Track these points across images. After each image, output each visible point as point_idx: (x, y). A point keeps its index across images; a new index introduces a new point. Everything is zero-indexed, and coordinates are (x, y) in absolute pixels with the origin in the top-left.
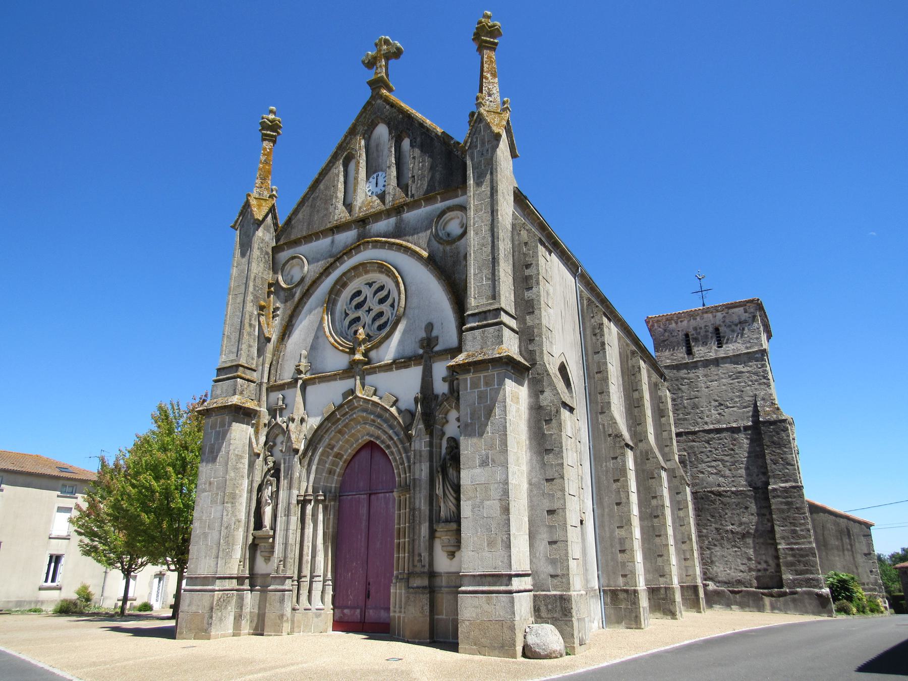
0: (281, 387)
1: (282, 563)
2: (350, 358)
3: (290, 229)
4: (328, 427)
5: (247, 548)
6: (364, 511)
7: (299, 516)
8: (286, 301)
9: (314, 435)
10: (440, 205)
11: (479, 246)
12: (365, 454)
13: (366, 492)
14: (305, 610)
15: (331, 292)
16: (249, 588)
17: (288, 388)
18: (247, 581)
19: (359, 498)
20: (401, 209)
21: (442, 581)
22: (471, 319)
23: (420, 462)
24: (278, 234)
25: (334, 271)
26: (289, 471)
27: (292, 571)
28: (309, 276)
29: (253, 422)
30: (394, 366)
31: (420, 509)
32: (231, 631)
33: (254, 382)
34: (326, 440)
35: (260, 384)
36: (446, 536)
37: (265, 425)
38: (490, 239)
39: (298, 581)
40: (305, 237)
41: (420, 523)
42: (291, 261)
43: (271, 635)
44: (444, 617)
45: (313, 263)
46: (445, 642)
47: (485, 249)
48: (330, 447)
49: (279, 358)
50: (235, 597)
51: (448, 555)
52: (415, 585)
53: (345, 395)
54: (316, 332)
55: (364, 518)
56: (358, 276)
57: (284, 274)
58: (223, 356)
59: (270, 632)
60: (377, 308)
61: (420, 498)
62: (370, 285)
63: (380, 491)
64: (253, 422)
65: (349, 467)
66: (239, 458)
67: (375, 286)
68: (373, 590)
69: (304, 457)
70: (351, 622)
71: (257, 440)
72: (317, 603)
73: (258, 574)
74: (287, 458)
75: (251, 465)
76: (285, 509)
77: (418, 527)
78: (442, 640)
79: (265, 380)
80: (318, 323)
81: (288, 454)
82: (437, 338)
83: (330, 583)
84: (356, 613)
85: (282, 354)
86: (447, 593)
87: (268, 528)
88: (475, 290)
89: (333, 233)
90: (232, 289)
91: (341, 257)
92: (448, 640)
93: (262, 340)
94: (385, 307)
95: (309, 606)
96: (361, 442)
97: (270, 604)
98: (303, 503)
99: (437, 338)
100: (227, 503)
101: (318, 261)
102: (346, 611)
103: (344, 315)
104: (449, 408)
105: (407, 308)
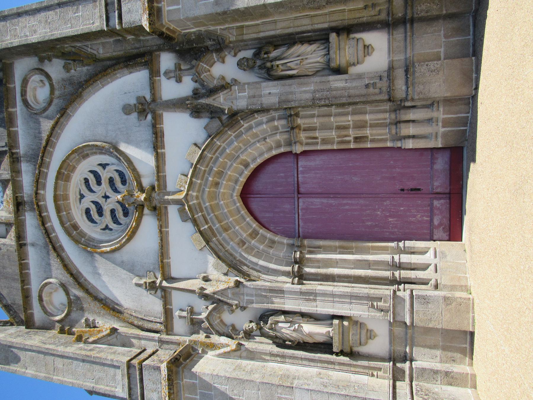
0: (168, 313)
1: (375, 304)
2: (147, 215)
3: (15, 307)
4: (217, 243)
5: (355, 363)
6: (317, 202)
7: (317, 283)
8: (82, 309)
9: (223, 261)
10: (19, 109)
11: (47, 26)
12: (255, 205)
13: (296, 199)
14: (436, 272)
15: (77, 242)
16: (408, 363)
17: (171, 305)
18: (399, 365)
19: (302, 209)
20: (15, 156)
21: (399, 60)
22: (111, 23)
23: (260, 96)
24: (17, 323)
25: (59, 241)
26: (262, 296)
27: (386, 291)
28: (60, 276)
29: (200, 352)
30: (159, 151)
31: (314, 92)
32: (469, 391)
33: (157, 350)
34: (232, 246)
35: (161, 342)
36: (345, 49)
37: (207, 337)
38: (43, 14)
39: (399, 283)
40: (23, 281)
41: (330, 90)
42: (45, 303)
43: (473, 317)
44: (442, 50)
45: (50, 271)
46: (474, 45)
47: (51, 18)
48: (241, 245)
49: (137, 317)
50: (421, 383)
51: (368, 54)
52: (404, 88)
53: (184, 218)
54: (116, 265)
55: (325, 201)
56: (68, 209)
57: (55, 314)
58: (117, 390)
59: (468, 319)
60: (105, 187)
61: (301, 93)
62: (82, 196)
63: (296, 179)
64: (200, 352)
65: (267, 225)
66: (239, 367)
67: (85, 191)
68: (411, 184)
69: (249, 276)
70: (450, 215)
71: (223, 346)
72: (428, 258)
73: (390, 350)
74: (246, 298)
75: (252, 356)
76: (308, 300)
77: (334, 92)
78: (471, 49)
79: (157, 335)
80: (108, 262)
81: (242, 297)
82: (138, 98)
83: (401, 244)
84: (438, 205)
85: (134, 314)
86: (413, 49)
87: (330, 329)
88: (86, 25)
89: (25, 245)
90: (47, 375)
91: (46, 229)
92: (471, 41)
93: (112, 339)
94: (105, 175)
95: (432, 268)
96: (239, 204)
97: (430, 320)
98: (301, 277)
99: (138, 98)
100: (292, 383)
101: (49, 264)
102: (436, 222)
103: (107, 231)
104: (208, 73)
105: (105, 140)
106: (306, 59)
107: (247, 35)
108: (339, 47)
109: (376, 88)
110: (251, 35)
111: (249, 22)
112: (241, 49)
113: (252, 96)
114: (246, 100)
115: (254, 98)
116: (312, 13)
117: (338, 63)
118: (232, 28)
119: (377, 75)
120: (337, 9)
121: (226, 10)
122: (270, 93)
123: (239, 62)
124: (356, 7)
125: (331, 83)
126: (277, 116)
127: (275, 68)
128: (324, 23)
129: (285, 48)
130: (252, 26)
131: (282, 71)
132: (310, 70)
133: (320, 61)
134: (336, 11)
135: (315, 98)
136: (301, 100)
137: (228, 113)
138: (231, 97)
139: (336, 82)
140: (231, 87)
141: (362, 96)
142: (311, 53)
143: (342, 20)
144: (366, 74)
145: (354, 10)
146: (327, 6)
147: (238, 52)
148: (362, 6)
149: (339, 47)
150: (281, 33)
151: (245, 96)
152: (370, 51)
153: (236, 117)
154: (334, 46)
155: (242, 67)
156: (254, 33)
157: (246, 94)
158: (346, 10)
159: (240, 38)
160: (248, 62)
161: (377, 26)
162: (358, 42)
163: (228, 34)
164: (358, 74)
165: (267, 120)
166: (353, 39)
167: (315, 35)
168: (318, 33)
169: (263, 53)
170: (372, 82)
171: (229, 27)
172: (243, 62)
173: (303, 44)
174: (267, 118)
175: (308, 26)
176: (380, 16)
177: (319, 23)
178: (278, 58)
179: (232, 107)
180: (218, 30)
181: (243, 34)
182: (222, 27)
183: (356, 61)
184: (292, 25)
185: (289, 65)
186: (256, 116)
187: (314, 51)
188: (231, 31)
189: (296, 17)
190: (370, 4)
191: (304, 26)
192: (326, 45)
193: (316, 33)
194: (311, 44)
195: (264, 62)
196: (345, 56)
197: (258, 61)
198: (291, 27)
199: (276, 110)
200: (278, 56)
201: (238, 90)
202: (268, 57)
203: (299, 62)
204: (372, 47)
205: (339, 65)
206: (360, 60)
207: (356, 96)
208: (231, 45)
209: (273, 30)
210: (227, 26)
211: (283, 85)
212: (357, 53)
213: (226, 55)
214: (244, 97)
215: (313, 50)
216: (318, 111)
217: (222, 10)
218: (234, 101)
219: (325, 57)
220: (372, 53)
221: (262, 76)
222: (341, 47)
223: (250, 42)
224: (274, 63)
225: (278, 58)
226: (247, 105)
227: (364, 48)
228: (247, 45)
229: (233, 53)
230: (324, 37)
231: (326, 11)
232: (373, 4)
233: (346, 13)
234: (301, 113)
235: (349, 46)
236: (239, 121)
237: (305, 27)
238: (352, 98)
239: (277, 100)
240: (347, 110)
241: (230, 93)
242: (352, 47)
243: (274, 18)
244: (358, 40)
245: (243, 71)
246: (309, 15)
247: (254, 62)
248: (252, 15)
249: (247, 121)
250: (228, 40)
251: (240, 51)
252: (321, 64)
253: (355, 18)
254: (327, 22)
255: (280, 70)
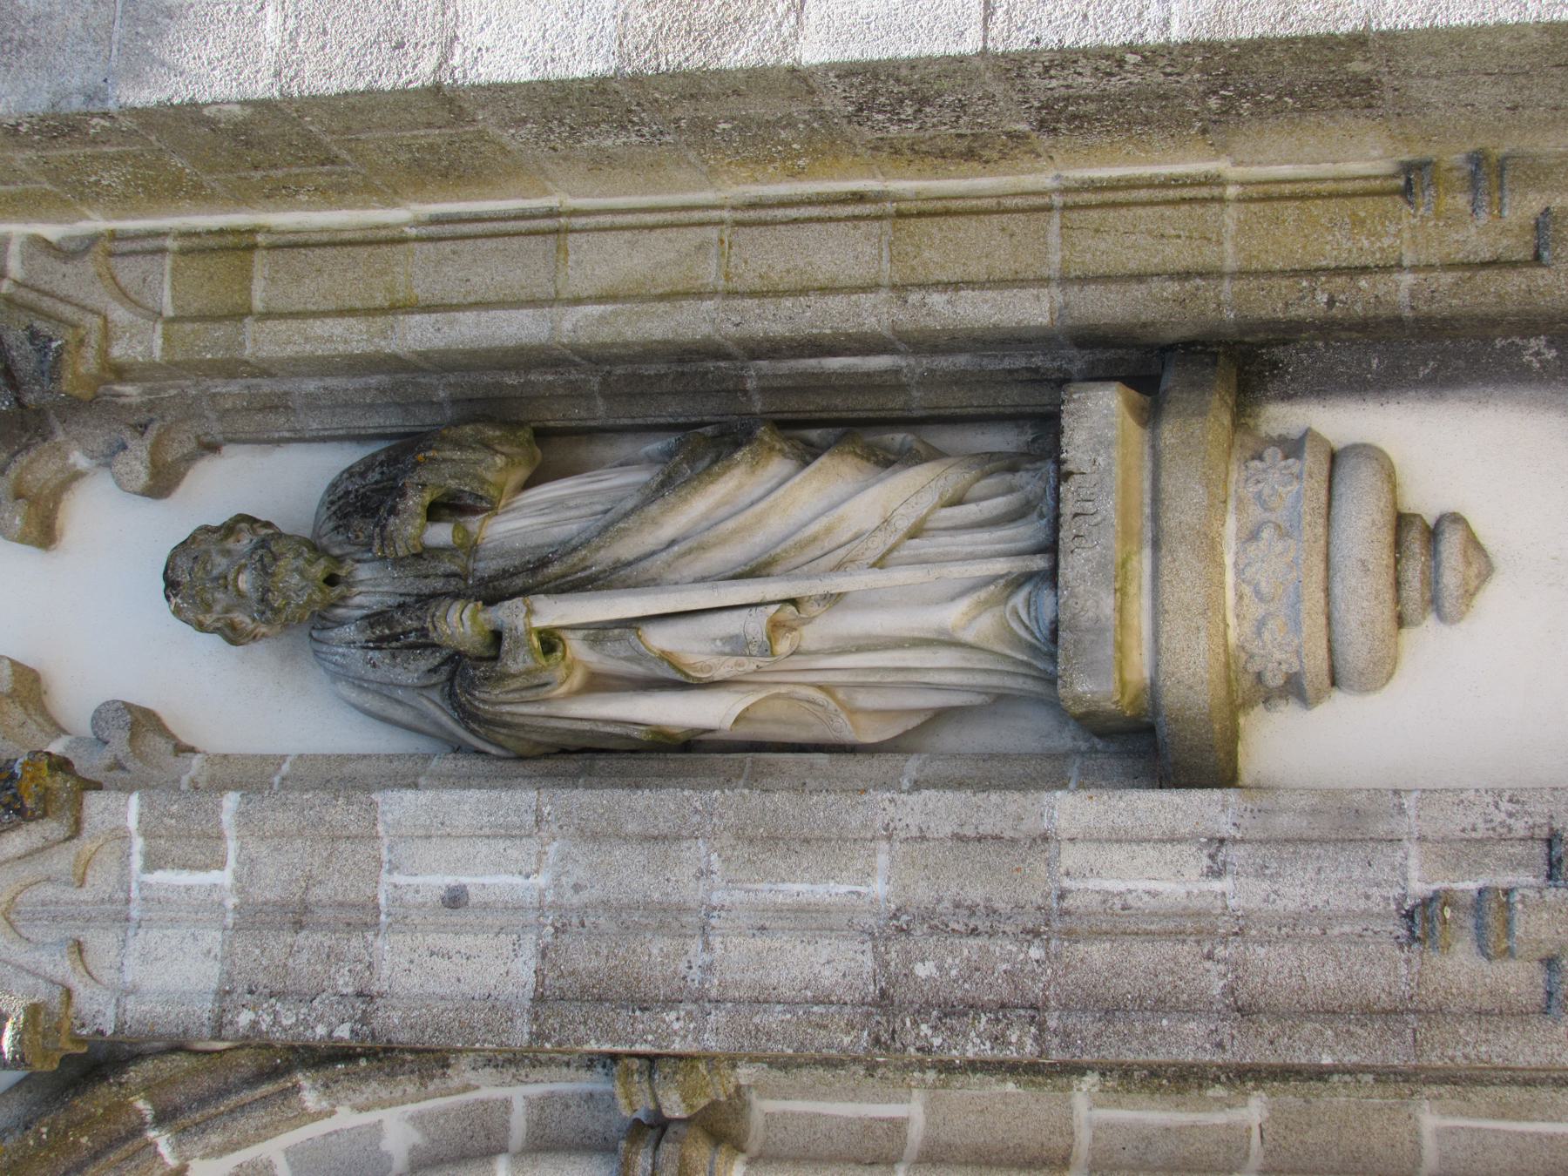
77: (1098, 953)
106: (833, 600)
107: (282, 326)
108: (1155, 518)
109: (1509, 953)
110: (319, 328)
111: (310, 206)
112: (216, 430)
113: (282, 906)
114: (213, 938)
115: (298, 926)
116: (907, 185)
117: (1139, 667)
118: (149, 246)
119: (1520, 827)
120: (1146, 171)
121: (77, 104)
122: (455, 899)
123: (184, 563)
124: (1325, 169)
125: (1071, 857)
126: (519, 1107)
127: (518, 662)
128: (1016, 282)
129: (640, 476)
130: (336, 242)
131: (598, 684)
132: (865, 700)
133: (968, 636)
134: (1131, 184)
135: (898, 993)
136: (760, 1001)
137: (19, 1061)
138: (71, 894)
139: (1118, 854)
140: (78, 805)
141: (1368, 1012)
142: (878, 545)
143: (1185, 275)
144: (1409, 802)
145: (1302, 194)
146: (1046, 140)
147: (190, 459)
148: (1385, 167)
149: (1155, 518)
150: (605, 335)
151: (208, 906)
152: (1450, 580)
153: (104, 1094)
154: (1109, 507)
155: (208, 607)
156: (341, 313)
157: (223, 878)
158: (1231, 191)
159: (210, 342)
160: (264, 571)
161: (1519, 351)
162: (1340, 489)
163: (98, 296)
164: (1333, 793)
165: (416, 1138)
166: (1293, 447)
167: (930, 380)
168: (962, 361)
169: (415, 502)
170: (1471, 885)
171: (114, 236)
172: (220, 563)
173: (808, 454)
174: (418, 1120)
175: (867, 300)
176: (1542, 278)
177: (970, 284)
178: (555, 569)
179: (68, 993)
180: (14, 248)
181: (239, 314)
182: (52, 231)
183: (1316, 663)
184: (709, 272)
185: (659, 639)
186: (311, 1098)
187: (916, 532)
188: (129, 272)
189: (752, 206)
190: (1453, 156)
191: (824, 291)
192: (1029, 482)
193: (943, 363)
194: (888, 461)
195: (426, 586)
196: (1213, 606)
197: (364, 572)
198: (699, 295)
199: (510, 1061)
200: (567, 548)
201: (147, 834)
202: (470, 548)
203: (754, 625)
204: (1473, 543)
205: (1154, 689)
206: (1356, 651)
207: (1306, 1014)
208: (131, 392)
209: (533, 303)
210: (96, 223)
211: (595, 837)
212: (1328, 591)
213: (76, 476)
214: (206, 907)
215: (903, 524)
216: (931, 1108)
217: (40, 104)
218: (101, 942)
219: (1019, 599)
220: (1469, 594)
221: (398, 713)
222: (1170, 521)
223: (311, 385)
224: (509, 614)
225: (555, 569)
226: (223, 994)
227: (1398, 545)
228: (277, 405)
229: (136, 463)
230: (1011, 398)
231: (1038, 178)
232: (1478, 159)
233: (1231, 217)
234: (763, 1107)
235: (1255, 513)
236: (137, 1131)
237: (836, 303)
238: (1271, 1030)
239: (524, 970)
240: (1219, 1118)
241: (62, 861)
242: (1283, 533)
243: (546, 192)
244: (1334, 458)
245: (216, 640)
246: (879, 197)
247: (331, 580)
248: (333, 160)
249: (215, 1139)
250: (90, 353)
251: (211, 448)
252: (975, 661)
253: (1312, 273)
254: (1043, 281)
255: (577, 679)
